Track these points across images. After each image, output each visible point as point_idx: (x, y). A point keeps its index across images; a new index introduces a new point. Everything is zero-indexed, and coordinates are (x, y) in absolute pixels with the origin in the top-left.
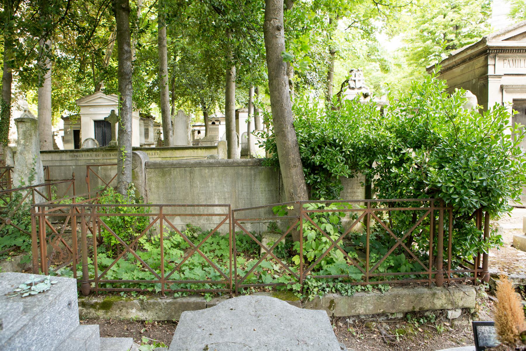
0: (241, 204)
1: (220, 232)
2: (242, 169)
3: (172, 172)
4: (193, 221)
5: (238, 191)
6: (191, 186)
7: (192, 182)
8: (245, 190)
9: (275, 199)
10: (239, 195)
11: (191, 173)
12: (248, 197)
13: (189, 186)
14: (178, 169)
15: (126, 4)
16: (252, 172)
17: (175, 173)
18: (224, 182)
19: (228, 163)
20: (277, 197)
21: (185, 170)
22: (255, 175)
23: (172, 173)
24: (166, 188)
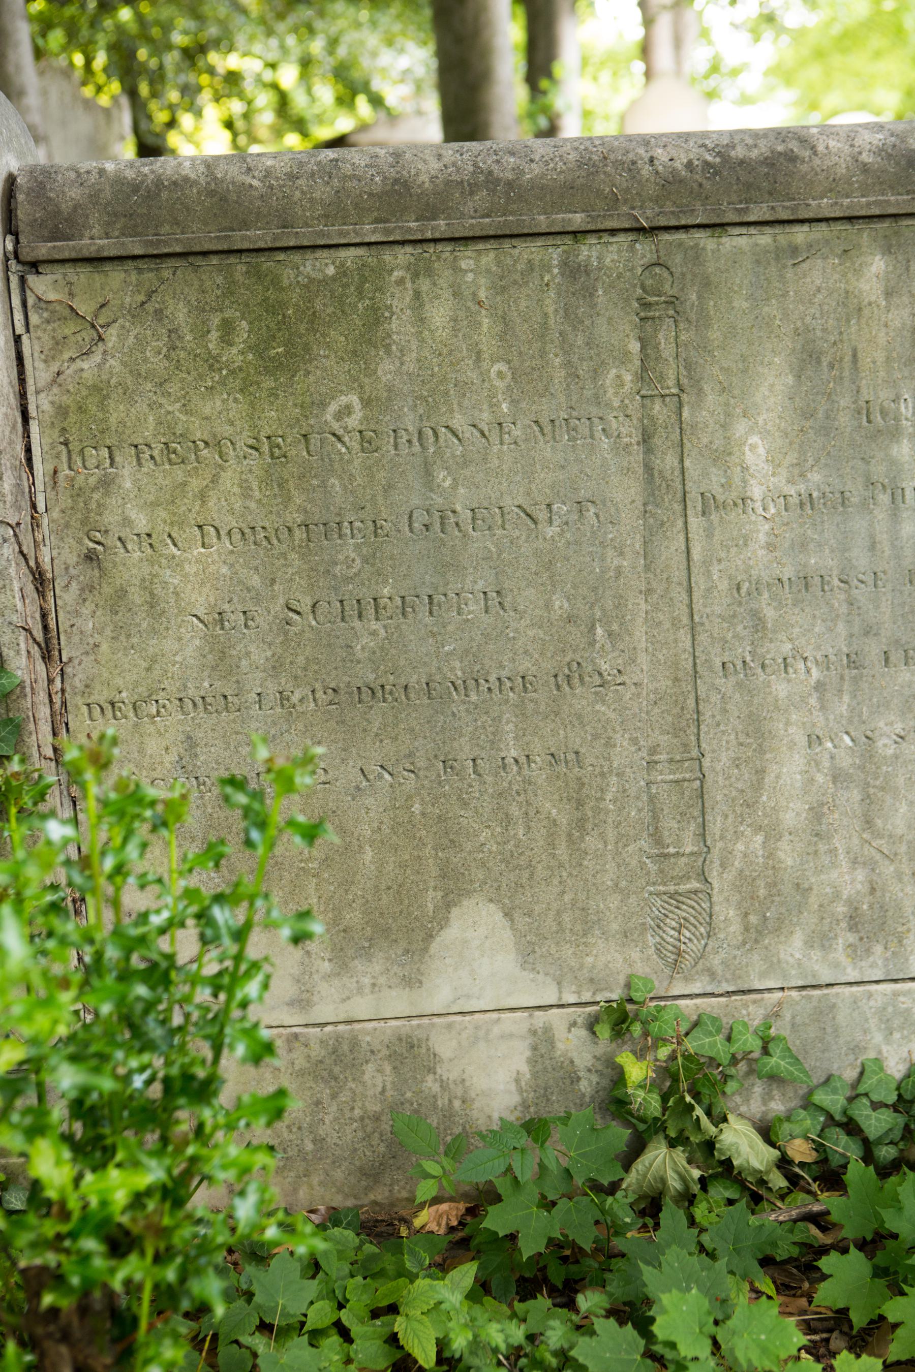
3: (398, 300)
4: (676, 962)
7: (668, 399)
11: (653, 307)
13: (626, 492)
14: (475, 266)
15: (227, 91)
17: (439, 315)
21: (574, 271)
23: (400, 326)
24: (321, 529)
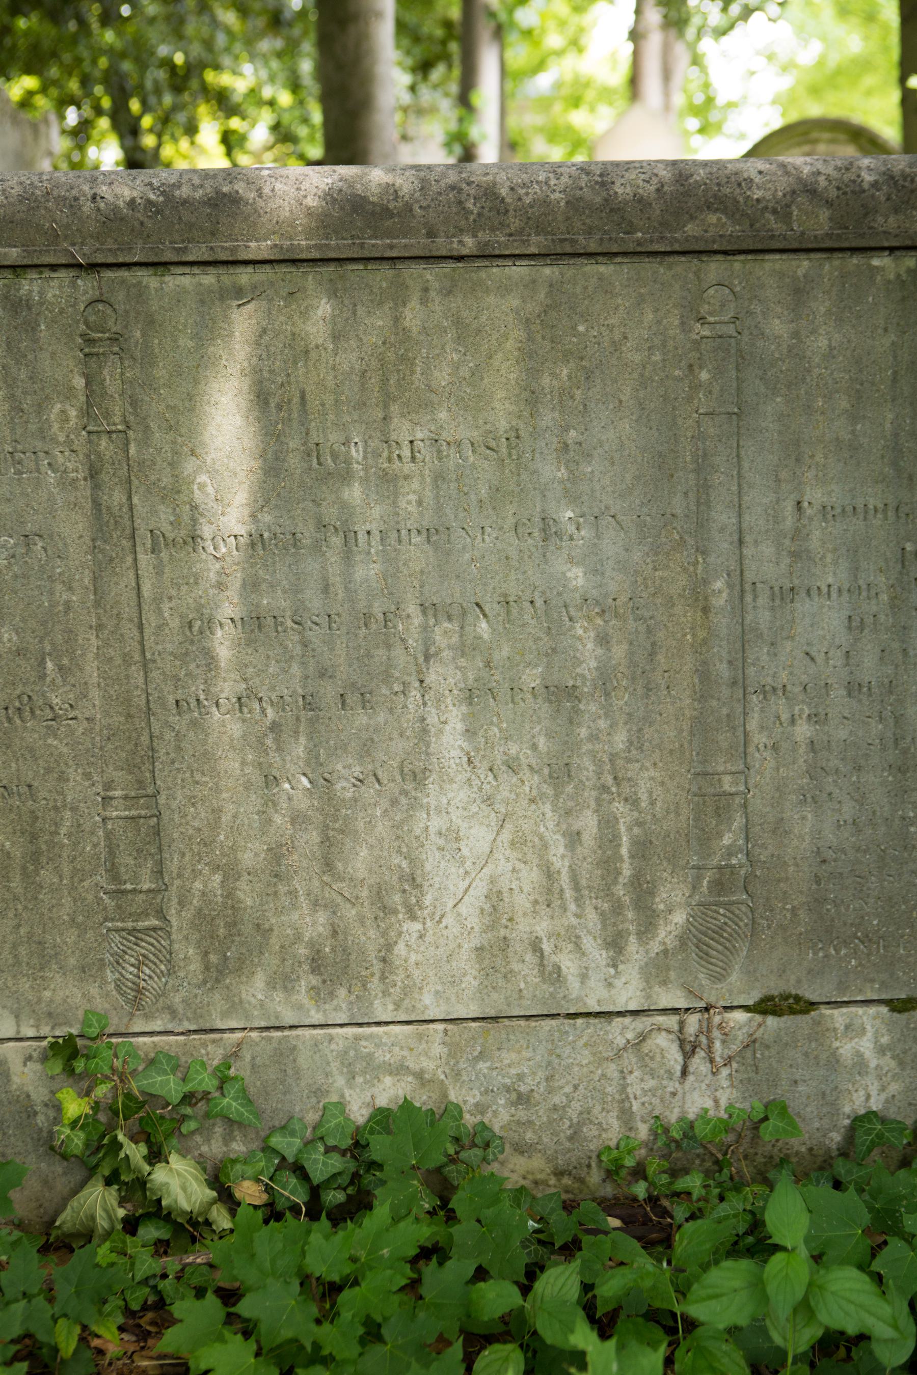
0: (764, 764)
1: (500, 1117)
2: (799, 293)
5: (741, 588)
6: (112, 531)
8: (832, 574)
10: (744, 639)
11: (98, 344)
12: (869, 667)
13: (73, 527)
18: (551, 471)
19: (612, 208)
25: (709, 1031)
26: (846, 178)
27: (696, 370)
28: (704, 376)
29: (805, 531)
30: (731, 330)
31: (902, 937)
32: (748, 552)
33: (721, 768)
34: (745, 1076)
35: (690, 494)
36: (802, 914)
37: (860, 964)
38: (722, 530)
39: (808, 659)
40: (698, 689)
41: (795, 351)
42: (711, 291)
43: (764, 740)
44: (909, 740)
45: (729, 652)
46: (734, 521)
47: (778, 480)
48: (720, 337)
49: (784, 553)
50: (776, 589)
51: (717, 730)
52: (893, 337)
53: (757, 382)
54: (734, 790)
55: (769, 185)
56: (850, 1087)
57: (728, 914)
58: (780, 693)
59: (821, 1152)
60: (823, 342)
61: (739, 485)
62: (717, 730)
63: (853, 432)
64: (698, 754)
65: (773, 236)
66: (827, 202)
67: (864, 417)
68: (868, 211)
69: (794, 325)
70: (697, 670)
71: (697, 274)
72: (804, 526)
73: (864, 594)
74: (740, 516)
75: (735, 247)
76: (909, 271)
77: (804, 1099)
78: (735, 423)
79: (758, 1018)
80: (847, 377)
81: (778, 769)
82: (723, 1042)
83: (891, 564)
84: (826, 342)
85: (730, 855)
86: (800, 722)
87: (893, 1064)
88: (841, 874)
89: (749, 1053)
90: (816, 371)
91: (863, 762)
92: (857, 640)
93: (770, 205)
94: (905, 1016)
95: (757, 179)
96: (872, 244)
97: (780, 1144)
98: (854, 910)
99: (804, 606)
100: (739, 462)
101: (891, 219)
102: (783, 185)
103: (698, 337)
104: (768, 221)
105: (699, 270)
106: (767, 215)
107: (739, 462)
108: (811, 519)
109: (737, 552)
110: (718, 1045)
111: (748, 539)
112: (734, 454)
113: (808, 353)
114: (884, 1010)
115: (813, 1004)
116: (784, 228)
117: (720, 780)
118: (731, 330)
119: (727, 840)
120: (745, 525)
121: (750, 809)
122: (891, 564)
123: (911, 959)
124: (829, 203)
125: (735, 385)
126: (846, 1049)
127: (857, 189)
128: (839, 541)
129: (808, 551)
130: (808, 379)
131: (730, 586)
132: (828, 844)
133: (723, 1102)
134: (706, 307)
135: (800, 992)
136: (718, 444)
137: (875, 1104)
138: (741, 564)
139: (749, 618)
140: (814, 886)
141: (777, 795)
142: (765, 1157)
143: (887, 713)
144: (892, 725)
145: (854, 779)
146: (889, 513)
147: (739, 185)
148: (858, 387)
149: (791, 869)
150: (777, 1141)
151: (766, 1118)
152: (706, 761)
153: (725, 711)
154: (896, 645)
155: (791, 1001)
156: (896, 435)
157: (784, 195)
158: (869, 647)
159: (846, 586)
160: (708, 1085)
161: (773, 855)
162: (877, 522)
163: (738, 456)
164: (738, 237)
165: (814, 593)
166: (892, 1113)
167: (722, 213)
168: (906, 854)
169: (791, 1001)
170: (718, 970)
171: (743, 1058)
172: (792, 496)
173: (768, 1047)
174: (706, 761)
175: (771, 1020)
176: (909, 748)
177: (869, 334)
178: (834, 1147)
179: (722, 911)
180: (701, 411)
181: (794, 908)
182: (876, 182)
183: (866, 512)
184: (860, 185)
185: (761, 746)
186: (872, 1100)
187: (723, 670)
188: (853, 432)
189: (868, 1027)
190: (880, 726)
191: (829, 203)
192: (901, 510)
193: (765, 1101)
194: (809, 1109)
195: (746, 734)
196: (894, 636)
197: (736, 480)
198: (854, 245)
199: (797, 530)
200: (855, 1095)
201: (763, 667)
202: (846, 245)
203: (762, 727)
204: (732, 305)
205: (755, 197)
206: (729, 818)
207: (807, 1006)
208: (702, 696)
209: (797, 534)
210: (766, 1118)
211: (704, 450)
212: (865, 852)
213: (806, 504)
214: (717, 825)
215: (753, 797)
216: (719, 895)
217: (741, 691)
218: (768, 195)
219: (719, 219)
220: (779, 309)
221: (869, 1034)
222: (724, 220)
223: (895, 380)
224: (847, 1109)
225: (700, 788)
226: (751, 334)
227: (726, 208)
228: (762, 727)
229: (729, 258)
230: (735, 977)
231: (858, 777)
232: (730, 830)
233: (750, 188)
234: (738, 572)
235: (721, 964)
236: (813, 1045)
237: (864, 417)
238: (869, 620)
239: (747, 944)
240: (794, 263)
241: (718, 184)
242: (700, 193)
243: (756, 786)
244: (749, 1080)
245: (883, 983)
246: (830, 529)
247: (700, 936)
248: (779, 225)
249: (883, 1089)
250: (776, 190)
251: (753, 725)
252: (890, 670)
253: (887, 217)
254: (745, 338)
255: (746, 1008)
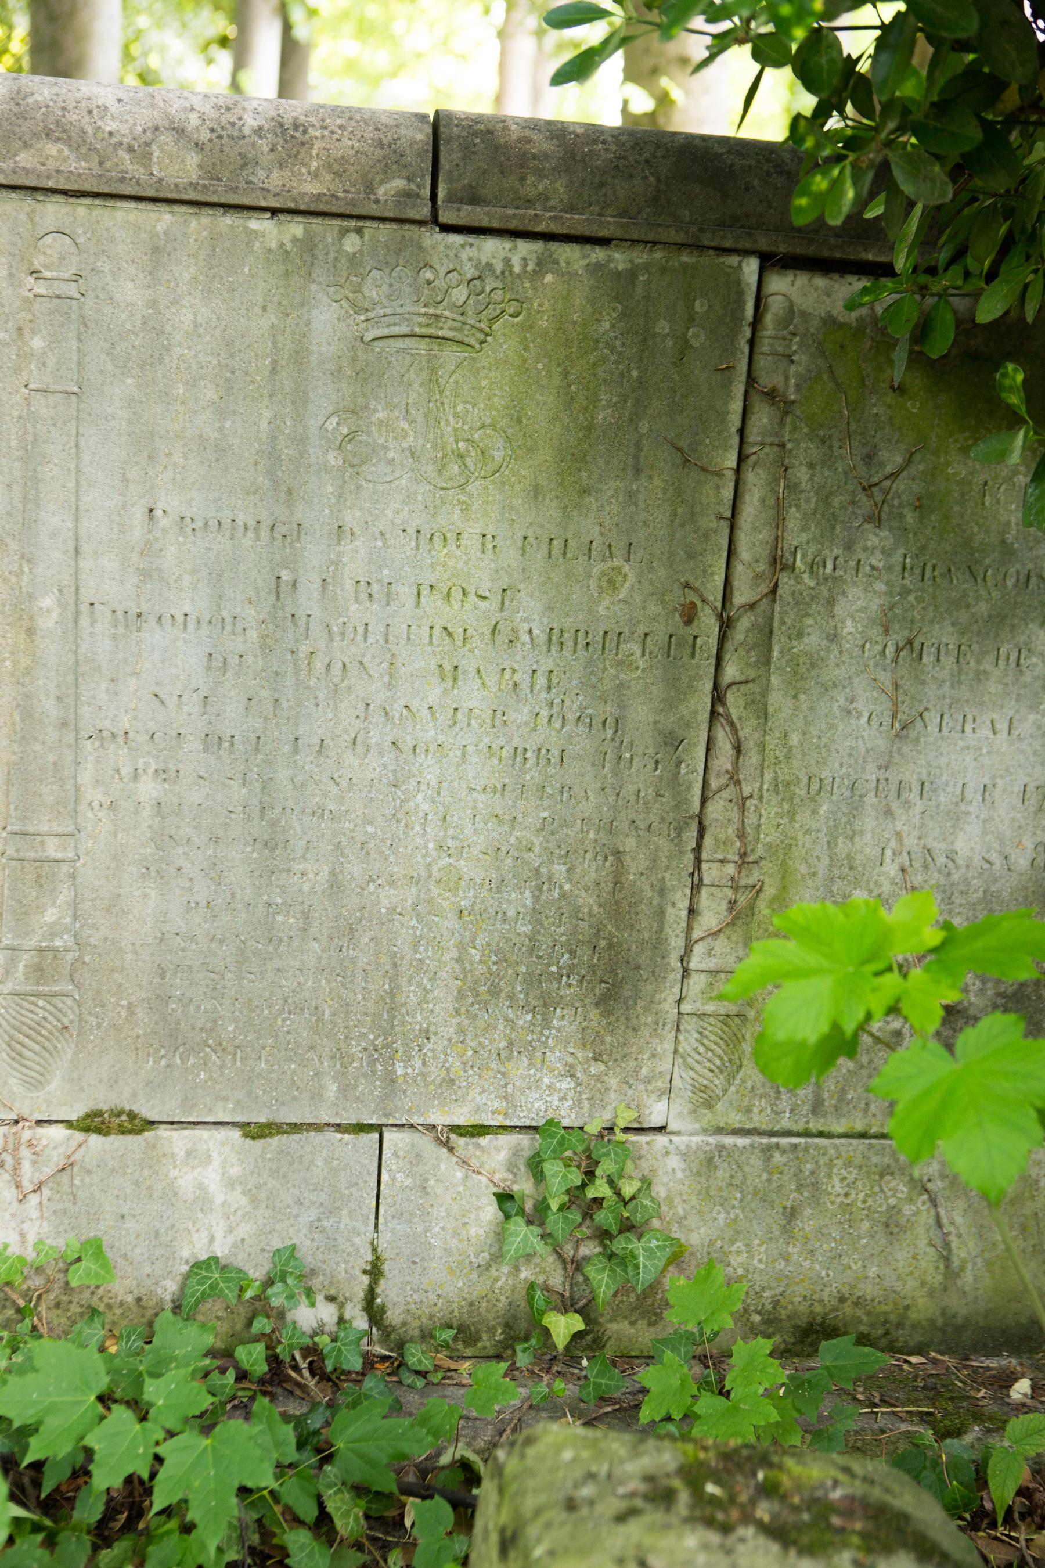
2: (158, 252)
5: (77, 608)
8: (189, 600)
9: (640, 777)
12: (232, 718)
16: (327, 321)
20: (673, 742)
22: (363, 370)
25: (16, 1149)
26: (224, 120)
27: (27, 335)
28: (37, 343)
29: (157, 546)
30: (72, 290)
31: (264, 1048)
32: (85, 564)
33: (44, 828)
34: (60, 1206)
35: (14, 487)
36: (141, 1013)
37: (211, 1078)
38: (53, 535)
39: (157, 702)
40: (18, 729)
41: (151, 324)
42: (48, 239)
43: (99, 797)
44: (278, 810)
45: (58, 686)
46: (70, 526)
47: (126, 480)
48: (58, 297)
49: (131, 570)
50: (120, 613)
51: (41, 781)
52: (273, 319)
53: (103, 356)
54: (59, 855)
55: (128, 117)
56: (190, 1227)
57: (48, 1007)
58: (121, 740)
59: (151, 1303)
60: (187, 317)
61: (77, 482)
62: (41, 781)
63: (221, 429)
64: (16, 808)
65: (124, 178)
66: (197, 144)
67: (235, 413)
68: (246, 162)
69: (151, 291)
70: (18, 705)
71: (30, 215)
72: (157, 539)
73: (228, 628)
74: (77, 519)
75: (75, 187)
76: (295, 240)
77: (132, 1238)
78: (74, 405)
79: (79, 1136)
80: (215, 362)
81: (115, 835)
82: (34, 1163)
83: (263, 594)
84: (190, 317)
85: (53, 935)
86: (144, 778)
87: (244, 1201)
88: (190, 967)
89: (65, 1177)
90: (177, 351)
91: (221, 833)
92: (217, 683)
93: (125, 141)
94: (260, 1143)
95: (115, 108)
96: (247, 201)
97: (101, 1291)
98: (206, 1012)
99: (154, 637)
100: (77, 454)
101: (275, 175)
102: (145, 117)
103: (30, 295)
104: (122, 160)
105: (34, 211)
106: (121, 153)
107: (77, 454)
108: (165, 531)
109: (73, 564)
110: (26, 1166)
111: (85, 548)
112: (73, 444)
113: (168, 328)
114: (236, 1134)
115: (153, 1123)
116: (142, 170)
117: (42, 843)
118: (72, 290)
119: (50, 916)
120: (82, 532)
121: (79, 880)
122: (263, 594)
123: (274, 1076)
124: (199, 147)
125: (75, 358)
126: (186, 1180)
127: (236, 133)
128: (198, 561)
129: (159, 570)
130: (167, 360)
131: (62, 605)
132: (175, 930)
133: (32, 1238)
134: (42, 258)
135: (136, 1109)
136: (52, 428)
137: (221, 1249)
138: (77, 579)
139: (84, 646)
140: (158, 980)
141: (114, 865)
142: (82, 1306)
143: (252, 776)
144: (258, 790)
145: (210, 852)
146: (263, 533)
147: (90, 112)
148: (229, 375)
149: (128, 957)
150: (98, 1287)
151: (79, 1259)
152: (26, 817)
153: (51, 758)
154: (265, 694)
155: (124, 1118)
156: (274, 438)
157: (145, 131)
158: (232, 693)
159: (206, 617)
160: (13, 1215)
161: (106, 939)
162: (248, 541)
163: (77, 446)
164: (80, 175)
165: (167, 620)
166: (240, 1261)
167: (64, 143)
168: (271, 949)
169: (124, 1118)
170: (34, 1074)
171: (58, 1184)
172: (143, 501)
173: (89, 1172)
174: (26, 817)
175: (94, 1139)
176: (279, 820)
177: (243, 312)
178: (168, 1298)
179: (41, 1003)
180: (32, 386)
181: (130, 1006)
182: (260, 128)
183: (234, 529)
184: (240, 130)
185: (96, 805)
186: (217, 1244)
187: (49, 707)
188: (221, 429)
189: (215, 1155)
190: (244, 791)
191: (199, 147)
192: (276, 529)
193: (83, 1238)
194: (138, 1251)
195: (77, 788)
196: (264, 683)
197: (73, 474)
198: (223, 200)
199: (148, 544)
200: (195, 1237)
201: (100, 708)
202: (214, 199)
203: (97, 781)
204: (75, 259)
205: (108, 129)
206: (53, 890)
207: (137, 1124)
208: (23, 738)
209: (147, 549)
210: (79, 1259)
211: (35, 435)
212: (221, 942)
213: (158, 513)
214: (37, 897)
215: (84, 865)
216: (38, 984)
217: (72, 735)
218: (124, 129)
219: (60, 151)
220: (132, 270)
221: (217, 1162)
222: (67, 152)
223: (274, 371)
224: (185, 1253)
225: (18, 851)
226: (97, 297)
227: (69, 138)
228: (97, 781)
229: (72, 200)
230: (55, 1085)
231: (215, 849)
232: (54, 904)
233: (102, 118)
234: (73, 589)
235: (37, 1068)
236: (146, 1173)
237: (235, 413)
238: (233, 661)
239: (73, 1046)
240: (153, 215)
241: (64, 109)
242: (39, 116)
243: (87, 853)
244: (65, 1211)
245: (238, 1103)
246: (188, 546)
247: (13, 1032)
248: (136, 167)
249: (230, 1231)
250: (135, 124)
251: (85, 777)
252: (258, 723)
253: (270, 171)
254: (89, 301)
255: (69, 1124)
